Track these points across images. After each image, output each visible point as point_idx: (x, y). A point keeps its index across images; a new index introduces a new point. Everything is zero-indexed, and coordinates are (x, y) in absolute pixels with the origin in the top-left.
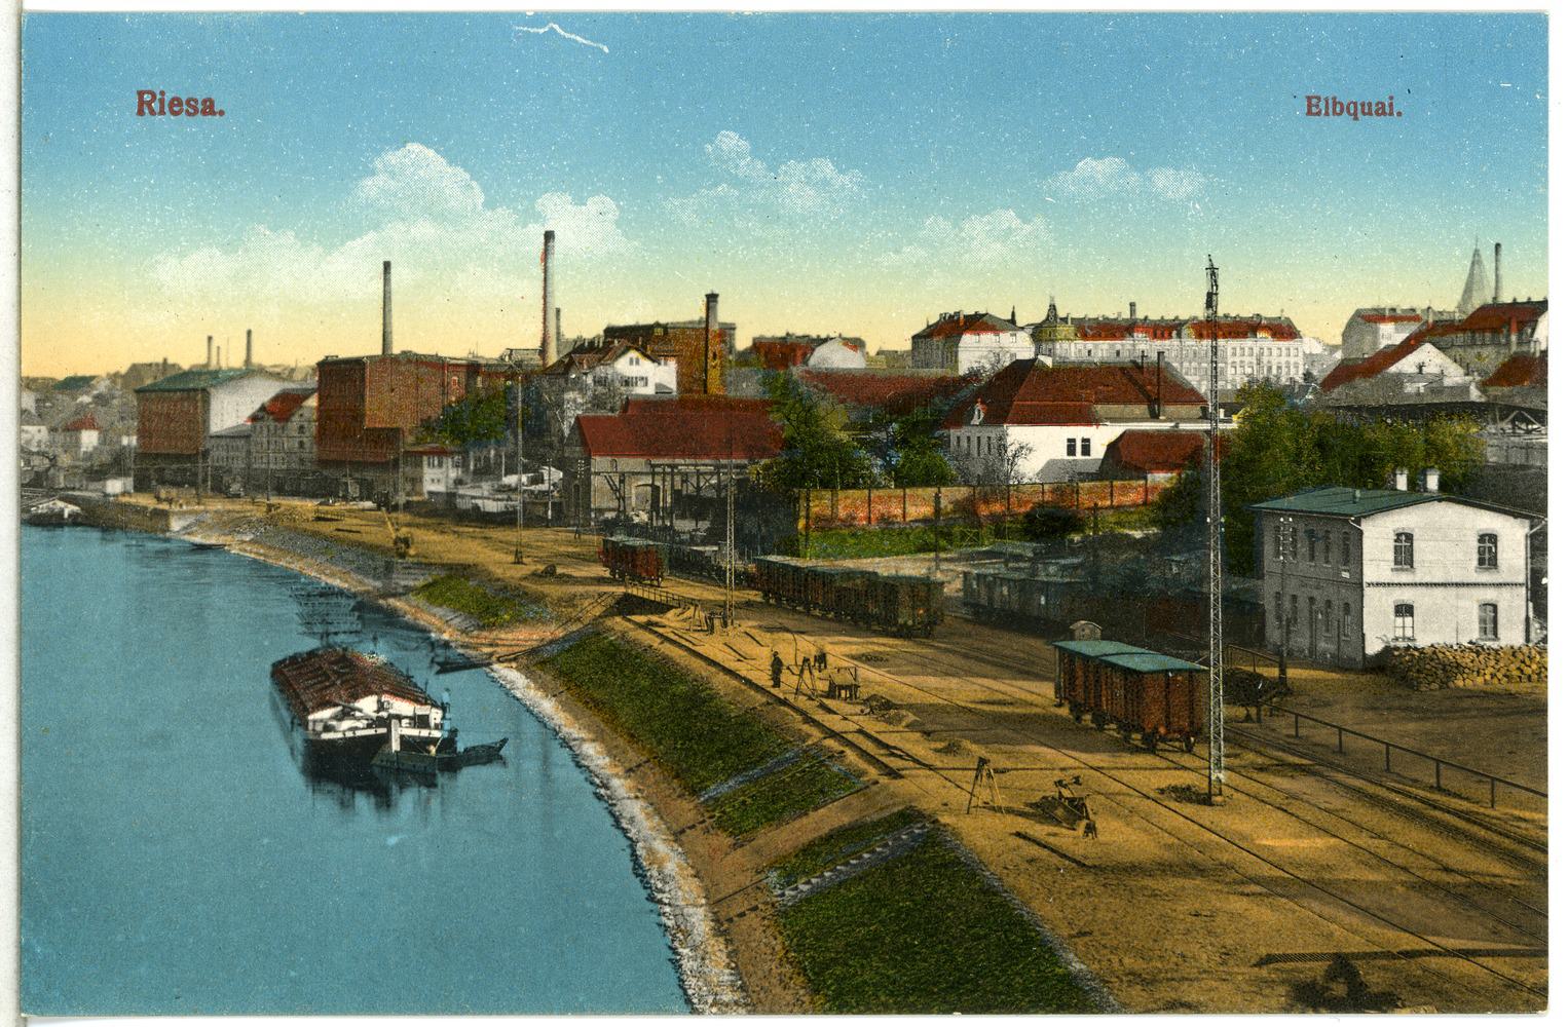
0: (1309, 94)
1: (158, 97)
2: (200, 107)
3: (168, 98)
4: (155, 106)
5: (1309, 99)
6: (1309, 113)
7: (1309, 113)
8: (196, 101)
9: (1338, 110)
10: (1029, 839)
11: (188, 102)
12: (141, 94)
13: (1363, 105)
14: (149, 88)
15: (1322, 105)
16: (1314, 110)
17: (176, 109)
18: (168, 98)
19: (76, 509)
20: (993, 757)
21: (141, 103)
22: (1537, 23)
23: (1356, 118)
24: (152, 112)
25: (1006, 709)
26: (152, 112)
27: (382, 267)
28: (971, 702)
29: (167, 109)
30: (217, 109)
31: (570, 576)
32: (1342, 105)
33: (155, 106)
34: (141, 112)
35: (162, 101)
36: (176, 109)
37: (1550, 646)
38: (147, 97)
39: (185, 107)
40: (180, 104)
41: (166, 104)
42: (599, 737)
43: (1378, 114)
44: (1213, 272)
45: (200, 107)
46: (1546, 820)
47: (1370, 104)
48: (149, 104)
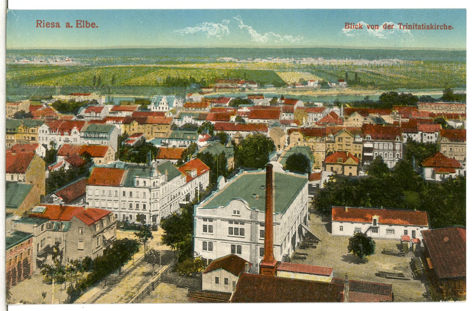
1: (43, 22)
4: (42, 25)
5: (77, 21)
6: (77, 27)
8: (54, 23)
16: (79, 26)
18: (426, 25)
19: (177, 160)
21: (38, 24)
23: (444, 24)
24: (41, 27)
25: (334, 62)
26: (41, 27)
28: (244, 203)
29: (45, 26)
30: (70, 26)
32: (446, 26)
33: (42, 25)
34: (37, 26)
36: (48, 26)
40: (49, 24)
48: (40, 24)
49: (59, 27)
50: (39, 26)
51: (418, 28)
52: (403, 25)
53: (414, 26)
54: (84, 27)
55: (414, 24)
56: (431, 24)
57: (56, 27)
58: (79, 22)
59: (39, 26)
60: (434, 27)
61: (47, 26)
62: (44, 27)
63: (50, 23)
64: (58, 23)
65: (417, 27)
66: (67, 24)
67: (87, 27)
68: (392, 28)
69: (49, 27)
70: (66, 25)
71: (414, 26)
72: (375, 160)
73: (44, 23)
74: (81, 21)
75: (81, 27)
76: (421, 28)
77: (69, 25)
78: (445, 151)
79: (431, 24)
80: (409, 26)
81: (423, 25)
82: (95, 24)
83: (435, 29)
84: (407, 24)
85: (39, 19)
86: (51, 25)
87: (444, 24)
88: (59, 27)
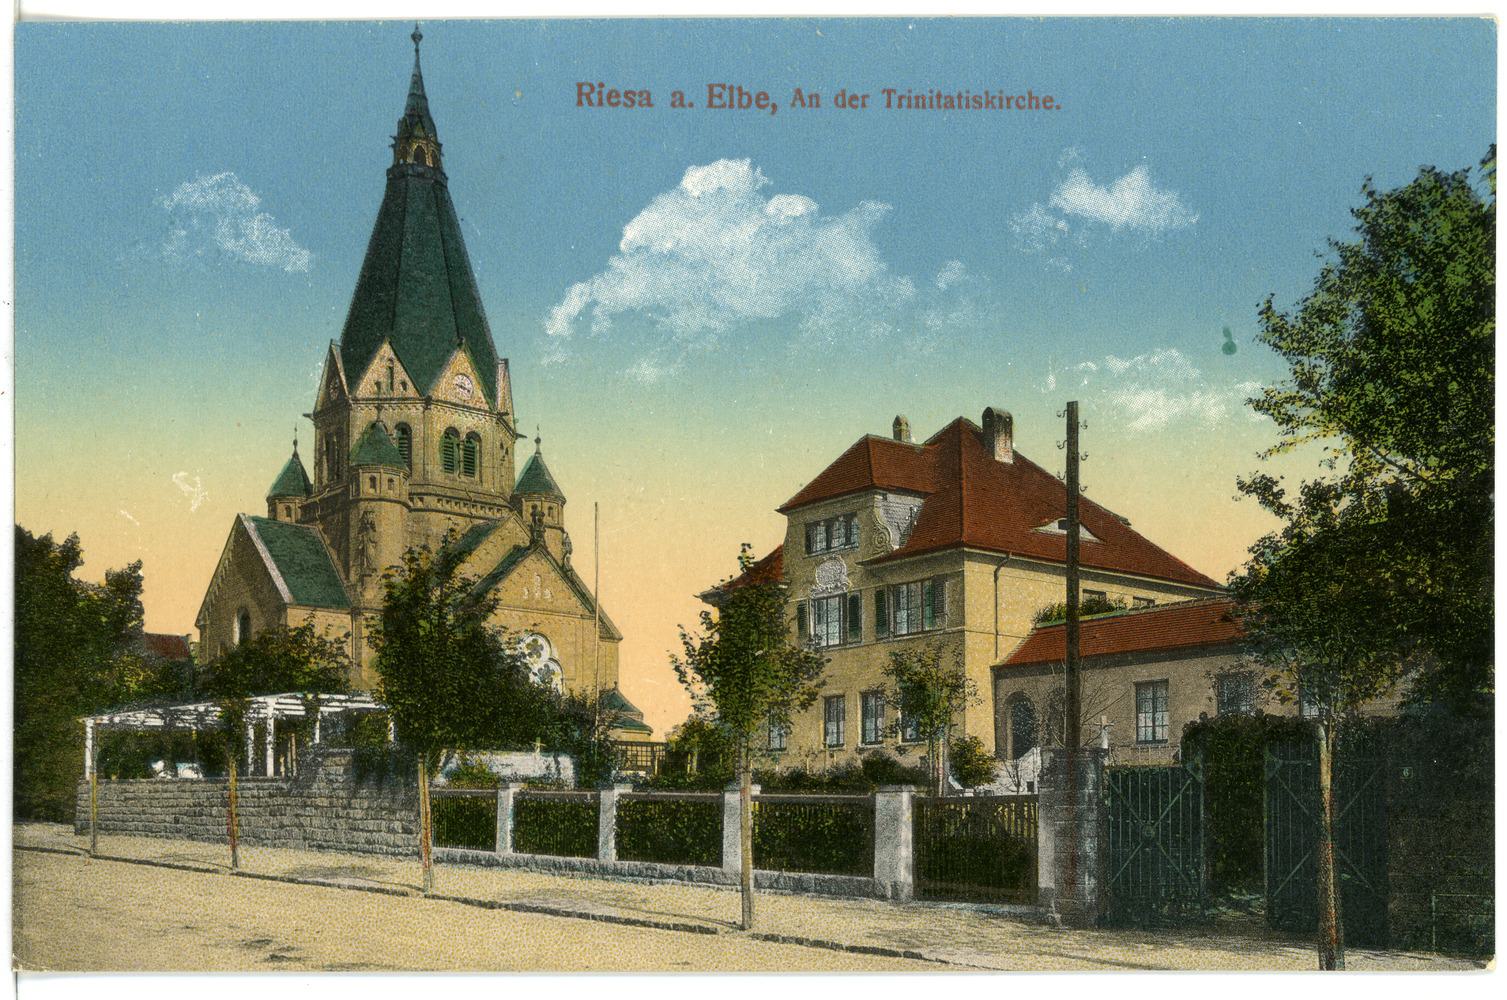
0: (580, 81)
1: (597, 89)
4: (594, 97)
7: (711, 105)
10: (1114, 964)
12: (580, 86)
13: (924, 106)
16: (716, 101)
17: (1048, 104)
18: (971, 96)
21: (580, 94)
23: (1030, 93)
24: (590, 103)
26: (590, 103)
29: (605, 101)
31: (283, 957)
33: (594, 97)
34: (580, 103)
36: (614, 100)
37: (1498, 172)
38: (586, 89)
40: (618, 95)
42: (825, 874)
47: (917, 106)
49: (650, 105)
50: (585, 101)
51: (945, 106)
52: (899, 93)
53: (931, 98)
54: (731, 106)
55: (931, 92)
56: (987, 93)
57: (640, 104)
58: (717, 90)
59: (585, 101)
60: (996, 102)
61: (1046, 107)
62: (601, 103)
63: (622, 93)
64: (817, 96)
65: (943, 101)
66: (674, 94)
67: (740, 105)
68: (864, 105)
69: (617, 104)
70: (671, 99)
71: (931, 98)
72: (989, 802)
73: (600, 93)
74: (723, 87)
75: (723, 106)
76: (956, 103)
77: (682, 99)
78: (547, 673)
79: (987, 93)
80: (917, 98)
81: (960, 97)
82: (1051, 100)
83: (1001, 106)
84: (1001, 92)
85: (715, 80)
86: (622, 99)
87: (1030, 93)
88: (650, 105)
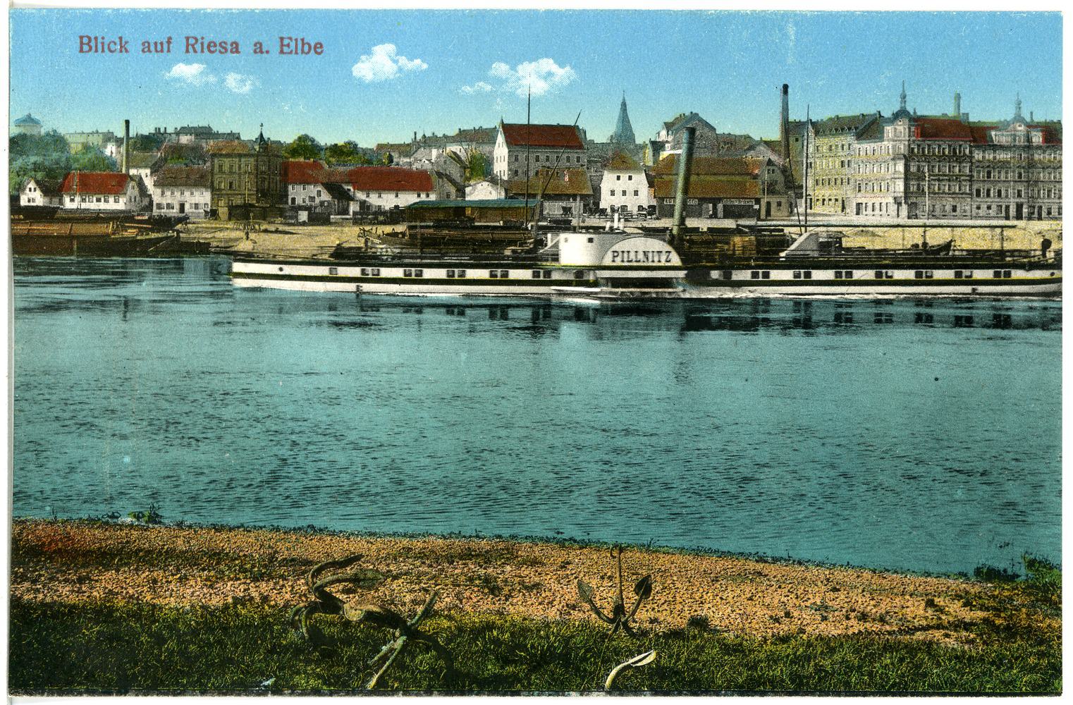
1: (200, 41)
2: (229, 47)
3: (107, 41)
4: (198, 47)
6: (282, 52)
9: (306, 48)
11: (220, 44)
14: (89, 35)
15: (293, 44)
17: (319, 50)
18: (107, 41)
20: (194, 210)
22: (1056, 18)
24: (195, 51)
26: (195, 51)
27: (124, 124)
30: (264, 50)
33: (198, 47)
34: (187, 51)
35: (202, 44)
39: (218, 48)
40: (215, 45)
41: (206, 45)
43: (232, 52)
44: (624, 105)
45: (229, 47)
46: (13, 222)
